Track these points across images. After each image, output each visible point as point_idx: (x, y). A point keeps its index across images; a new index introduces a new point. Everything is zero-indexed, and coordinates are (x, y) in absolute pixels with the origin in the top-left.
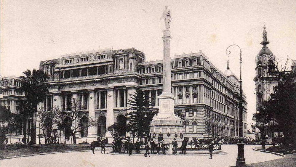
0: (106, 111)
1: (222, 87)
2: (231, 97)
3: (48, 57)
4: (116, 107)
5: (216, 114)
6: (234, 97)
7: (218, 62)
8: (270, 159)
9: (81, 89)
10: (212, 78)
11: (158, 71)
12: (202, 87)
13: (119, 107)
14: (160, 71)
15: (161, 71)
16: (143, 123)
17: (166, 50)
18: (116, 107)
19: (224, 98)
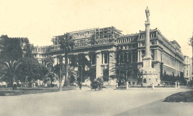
0: (96, 66)
1: (166, 48)
2: (174, 56)
3: (68, 32)
4: (102, 63)
5: (165, 67)
6: (175, 56)
7: (168, 35)
8: (22, 97)
9: (80, 53)
10: (163, 45)
11: (120, 42)
12: (158, 50)
13: (104, 64)
14: (143, 38)
15: (144, 38)
16: (22, 83)
17: (147, 25)
18: (102, 63)
19: (170, 56)
